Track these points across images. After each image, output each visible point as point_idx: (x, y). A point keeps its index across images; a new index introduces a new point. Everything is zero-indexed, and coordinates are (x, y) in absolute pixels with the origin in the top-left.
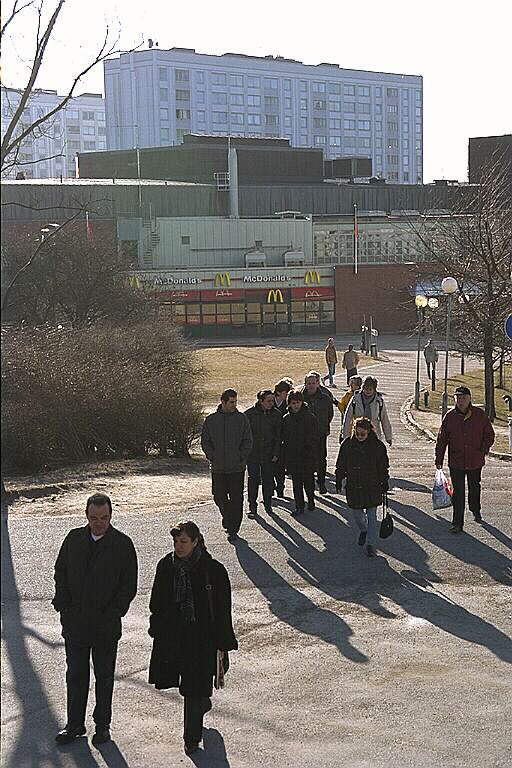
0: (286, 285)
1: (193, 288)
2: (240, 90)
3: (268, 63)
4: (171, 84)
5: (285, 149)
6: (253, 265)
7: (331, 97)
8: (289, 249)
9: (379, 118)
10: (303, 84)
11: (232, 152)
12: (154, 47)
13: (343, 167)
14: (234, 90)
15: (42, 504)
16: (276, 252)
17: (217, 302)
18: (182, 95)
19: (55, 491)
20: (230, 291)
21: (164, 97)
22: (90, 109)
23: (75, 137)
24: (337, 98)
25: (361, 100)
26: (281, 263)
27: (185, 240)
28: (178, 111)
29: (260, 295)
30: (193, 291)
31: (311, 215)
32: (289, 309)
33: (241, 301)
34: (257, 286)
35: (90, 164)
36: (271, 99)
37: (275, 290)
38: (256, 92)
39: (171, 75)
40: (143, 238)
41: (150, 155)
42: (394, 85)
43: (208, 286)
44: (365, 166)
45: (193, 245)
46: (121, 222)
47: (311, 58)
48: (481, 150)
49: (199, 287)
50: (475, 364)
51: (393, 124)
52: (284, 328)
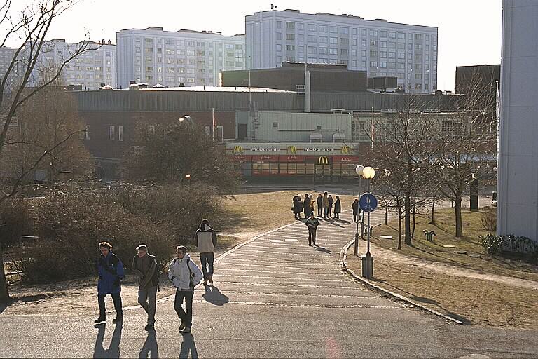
0: (330, 154)
1: (274, 154)
2: (326, 34)
3: (342, 18)
4: (283, 30)
5: (344, 71)
6: (315, 141)
7: (382, 39)
8: (337, 131)
9: (410, 51)
10: (385, 33)
11: (307, 73)
12: (274, 8)
13: (379, 82)
14: (322, 34)
15: (29, 306)
16: (329, 133)
17: (288, 163)
18: (290, 37)
19: (43, 297)
20: (296, 156)
21: (279, 36)
22: (240, 43)
23: (231, 59)
24: (385, 39)
25: (400, 41)
26: (331, 140)
27: (275, 125)
28: (287, 46)
29: (313, 159)
30: (275, 156)
31: (352, 111)
32: (332, 167)
33: (302, 162)
34: (312, 154)
35: (229, 79)
36: (344, 40)
37: (323, 156)
38: (336, 35)
39: (284, 25)
40: (250, 121)
41: (245, 74)
42: (418, 32)
43: (284, 153)
44: (392, 81)
45: (279, 128)
46: (238, 113)
47: (369, 16)
48: (463, 74)
49: (279, 154)
50: (448, 203)
51: (419, 56)
52: (329, 179)
